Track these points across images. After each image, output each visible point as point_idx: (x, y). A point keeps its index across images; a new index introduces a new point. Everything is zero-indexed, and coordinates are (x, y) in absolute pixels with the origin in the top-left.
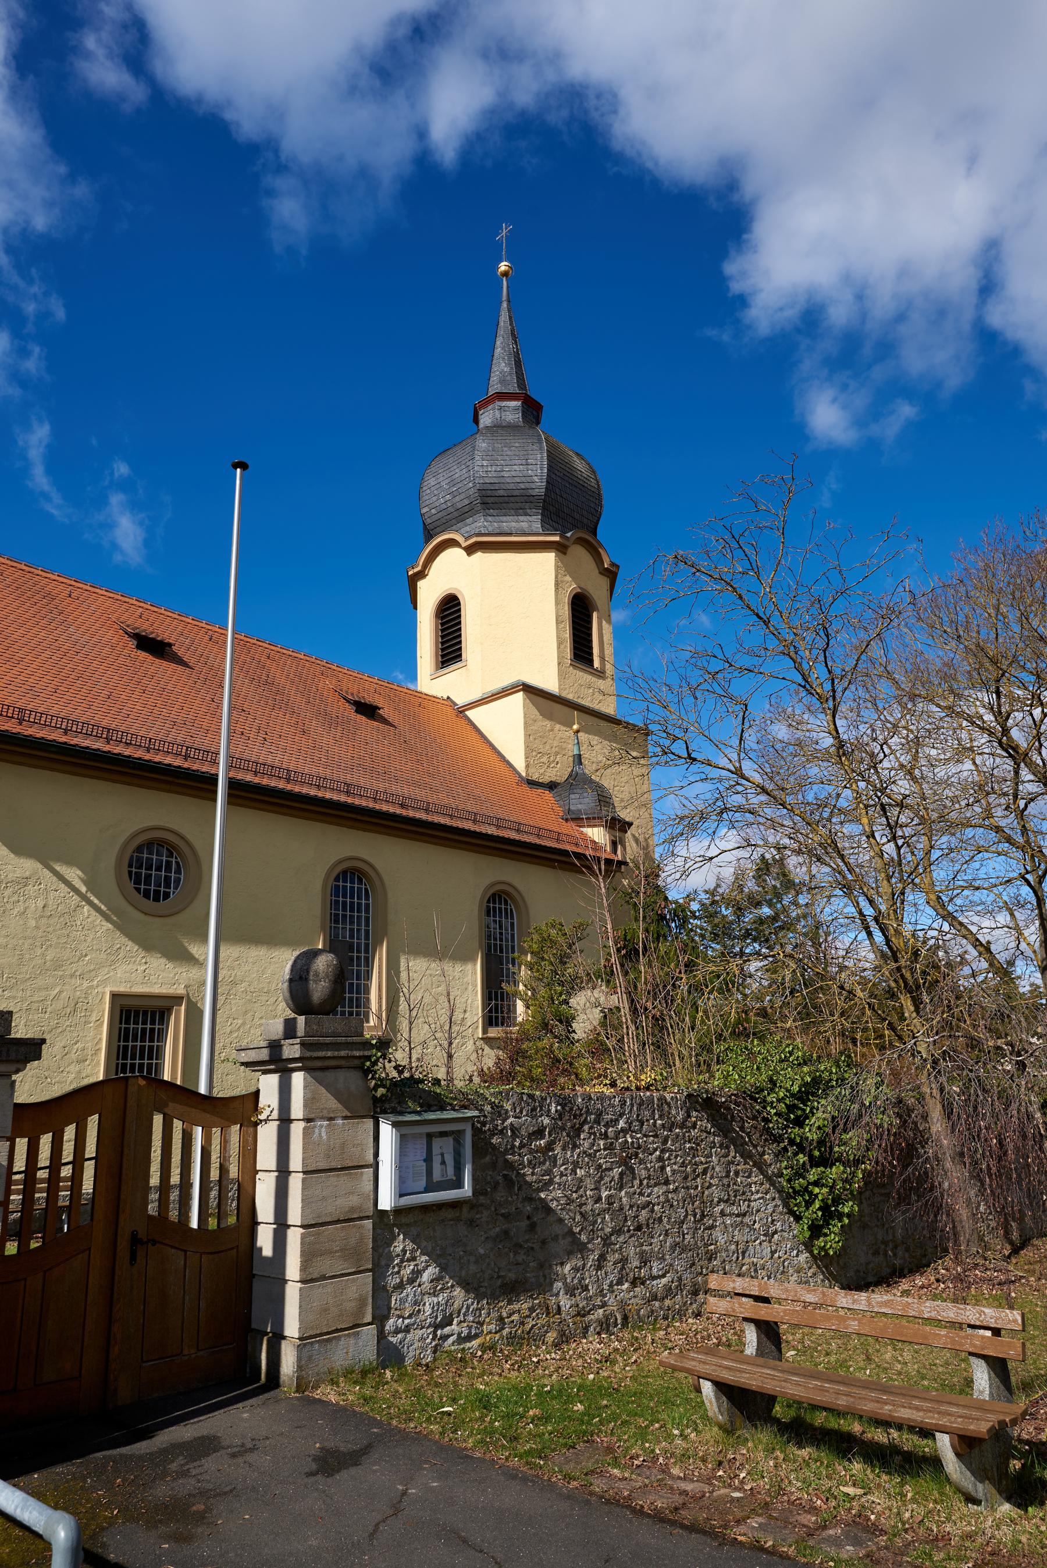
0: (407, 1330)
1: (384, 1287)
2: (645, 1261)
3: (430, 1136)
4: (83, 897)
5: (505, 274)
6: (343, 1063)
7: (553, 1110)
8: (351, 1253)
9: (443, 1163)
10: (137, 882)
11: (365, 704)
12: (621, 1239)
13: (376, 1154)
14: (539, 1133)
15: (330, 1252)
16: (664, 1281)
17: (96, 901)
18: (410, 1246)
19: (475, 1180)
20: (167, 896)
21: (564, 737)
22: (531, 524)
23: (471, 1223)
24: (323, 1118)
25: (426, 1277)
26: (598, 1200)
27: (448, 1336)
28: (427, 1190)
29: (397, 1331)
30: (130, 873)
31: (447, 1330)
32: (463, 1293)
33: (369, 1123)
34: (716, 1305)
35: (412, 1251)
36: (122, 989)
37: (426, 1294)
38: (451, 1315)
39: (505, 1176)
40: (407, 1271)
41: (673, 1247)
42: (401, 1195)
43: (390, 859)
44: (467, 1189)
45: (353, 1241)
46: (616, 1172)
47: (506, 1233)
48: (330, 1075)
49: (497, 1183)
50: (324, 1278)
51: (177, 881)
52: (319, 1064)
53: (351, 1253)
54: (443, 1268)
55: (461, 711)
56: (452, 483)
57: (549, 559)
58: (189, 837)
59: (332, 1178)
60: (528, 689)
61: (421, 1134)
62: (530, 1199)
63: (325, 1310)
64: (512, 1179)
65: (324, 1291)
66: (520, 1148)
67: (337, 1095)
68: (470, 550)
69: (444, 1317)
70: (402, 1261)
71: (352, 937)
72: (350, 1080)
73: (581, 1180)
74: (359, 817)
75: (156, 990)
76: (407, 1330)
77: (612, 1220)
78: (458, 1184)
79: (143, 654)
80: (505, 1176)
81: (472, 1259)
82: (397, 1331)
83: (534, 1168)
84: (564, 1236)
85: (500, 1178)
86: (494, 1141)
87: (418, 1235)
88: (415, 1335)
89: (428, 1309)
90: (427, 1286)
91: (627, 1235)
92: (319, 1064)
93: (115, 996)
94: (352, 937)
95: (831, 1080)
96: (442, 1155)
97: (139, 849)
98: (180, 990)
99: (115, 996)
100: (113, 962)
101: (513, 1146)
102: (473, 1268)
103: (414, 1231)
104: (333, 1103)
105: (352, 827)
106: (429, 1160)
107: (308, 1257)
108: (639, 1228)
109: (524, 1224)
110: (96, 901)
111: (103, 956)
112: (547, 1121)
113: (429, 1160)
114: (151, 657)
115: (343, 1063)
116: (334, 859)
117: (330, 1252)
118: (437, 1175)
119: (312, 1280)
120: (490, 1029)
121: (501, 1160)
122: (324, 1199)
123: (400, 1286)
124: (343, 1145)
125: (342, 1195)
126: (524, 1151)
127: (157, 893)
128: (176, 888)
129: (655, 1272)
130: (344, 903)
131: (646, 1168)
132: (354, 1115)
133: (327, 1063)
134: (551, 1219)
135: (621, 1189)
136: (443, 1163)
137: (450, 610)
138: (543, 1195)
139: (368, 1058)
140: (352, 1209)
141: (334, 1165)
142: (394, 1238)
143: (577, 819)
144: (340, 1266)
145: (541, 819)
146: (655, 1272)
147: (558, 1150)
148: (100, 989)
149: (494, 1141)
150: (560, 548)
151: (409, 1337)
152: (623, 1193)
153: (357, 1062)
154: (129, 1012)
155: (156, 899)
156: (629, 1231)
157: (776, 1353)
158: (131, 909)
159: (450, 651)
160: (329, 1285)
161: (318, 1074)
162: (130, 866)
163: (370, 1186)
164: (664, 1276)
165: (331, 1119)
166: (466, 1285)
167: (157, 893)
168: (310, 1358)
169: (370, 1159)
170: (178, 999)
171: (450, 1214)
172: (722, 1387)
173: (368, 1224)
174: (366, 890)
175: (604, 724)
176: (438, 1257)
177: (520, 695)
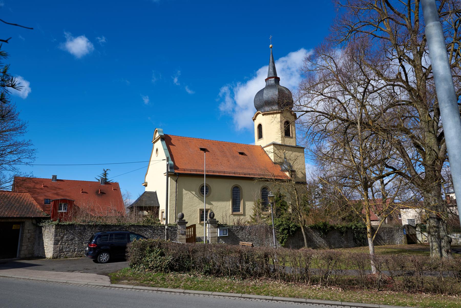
5: (271, 48)
8: (216, 240)
21: (281, 153)
22: (275, 107)
43: (243, 185)
53: (216, 240)
55: (263, 148)
56: (260, 100)
57: (279, 115)
60: (274, 144)
64: (234, 234)
68: (263, 115)
72: (214, 225)
98: (209, 208)
107: (211, 240)
125: (214, 235)
137: (260, 126)
143: (283, 171)
145: (277, 171)
150: (281, 113)
159: (260, 136)
175: (292, 148)
177: (272, 147)
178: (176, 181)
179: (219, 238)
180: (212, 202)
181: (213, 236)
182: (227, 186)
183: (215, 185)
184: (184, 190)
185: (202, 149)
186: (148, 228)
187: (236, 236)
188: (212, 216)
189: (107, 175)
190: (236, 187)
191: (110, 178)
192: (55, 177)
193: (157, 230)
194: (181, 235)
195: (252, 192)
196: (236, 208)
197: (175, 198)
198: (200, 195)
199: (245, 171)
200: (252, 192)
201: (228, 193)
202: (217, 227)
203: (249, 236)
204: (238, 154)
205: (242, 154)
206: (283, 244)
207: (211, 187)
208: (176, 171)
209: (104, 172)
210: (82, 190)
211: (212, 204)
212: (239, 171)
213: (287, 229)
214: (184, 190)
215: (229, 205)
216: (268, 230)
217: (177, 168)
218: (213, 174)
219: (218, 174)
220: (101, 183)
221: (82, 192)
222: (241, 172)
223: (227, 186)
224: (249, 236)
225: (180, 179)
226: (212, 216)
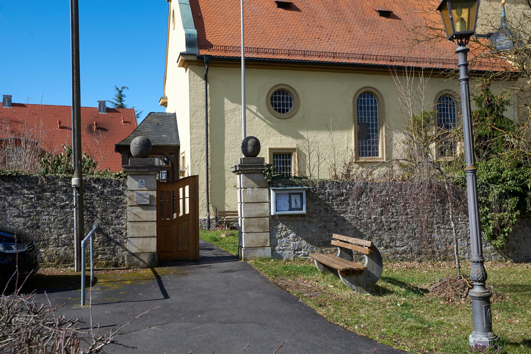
0: (284, 250)
1: (275, 237)
2: (392, 240)
3: (290, 194)
4: (255, 114)
6: (256, 171)
7: (348, 187)
8: (263, 227)
9: (296, 202)
10: (276, 106)
11: (384, 11)
12: (381, 232)
13: (270, 199)
14: (342, 195)
15: (254, 226)
16: (402, 248)
17: (260, 115)
18: (284, 227)
19: (307, 208)
20: (287, 110)
23: (309, 222)
24: (250, 188)
25: (291, 236)
26: (370, 218)
27: (300, 254)
28: (289, 210)
29: (280, 250)
30: (272, 103)
31: (300, 252)
32: (306, 242)
33: (267, 190)
34: (333, 242)
35: (285, 228)
36: (273, 146)
37: (289, 241)
38: (301, 248)
39: (325, 208)
40: (284, 233)
41: (408, 238)
42: (277, 211)
44: (304, 211)
45: (262, 223)
46: (380, 209)
47: (325, 226)
48: (252, 175)
49: (321, 210)
50: (252, 232)
51: (291, 104)
52: (247, 172)
53: (263, 227)
54: (298, 234)
58: (293, 86)
59: (254, 205)
61: (286, 193)
62: (336, 216)
63: (253, 241)
64: (328, 209)
65: (250, 236)
66: (332, 199)
67: (254, 181)
69: (298, 248)
70: (281, 231)
71: (369, 121)
72: (259, 177)
73: (361, 211)
74: (367, 69)
75: (286, 146)
76: (284, 250)
77: (376, 226)
78: (302, 209)
79: (280, 10)
80: (325, 208)
81: (310, 233)
82: (280, 250)
83: (338, 206)
84: (352, 229)
85: (322, 209)
86: (320, 197)
87: (287, 224)
88: (286, 252)
89: (292, 245)
90: (291, 239)
91: (384, 231)
92: (247, 172)
93: (270, 149)
94: (369, 121)
95: (507, 177)
96: (296, 200)
97: (275, 93)
98: (294, 146)
99: (270, 149)
100: (269, 137)
101: (329, 199)
102: (310, 235)
103: (286, 222)
104: (253, 183)
105: (366, 74)
106: (290, 202)
108: (390, 229)
109: (333, 224)
110: (260, 115)
111: (265, 135)
112: (345, 191)
113: (290, 202)
114: (284, 10)
115: (256, 171)
116: (358, 89)
117: (254, 226)
118: (293, 206)
119: (248, 233)
120: (361, 158)
121: (323, 203)
122: (251, 211)
123: (281, 238)
124: (257, 196)
125: (257, 210)
126: (334, 200)
127: (283, 110)
128: (291, 107)
129: (398, 244)
130: (368, 107)
131: (396, 209)
132: (261, 187)
133: (249, 172)
134: (345, 223)
135: (382, 215)
136: (296, 202)
138: (342, 215)
139: (264, 170)
140: (261, 214)
141: (254, 201)
142: (279, 224)
144: (258, 230)
146: (398, 244)
147: (350, 201)
148: (265, 147)
149: (320, 197)
151: (284, 252)
152: (383, 217)
153: (260, 171)
154: (277, 155)
155: (283, 112)
156: (385, 230)
157: (350, 258)
158: (273, 117)
160: (254, 235)
161: (247, 175)
162: (272, 100)
163: (268, 208)
164: (403, 246)
165: (253, 188)
166: (307, 240)
167: (283, 110)
168: (248, 253)
169: (267, 200)
170: (294, 150)
171: (301, 218)
172: (319, 263)
173: (268, 219)
174: (375, 100)
176: (293, 230)
178: (206, 79)
179: (274, 220)
180: (302, 133)
181: (253, 214)
182: (342, 92)
183: (304, 86)
184: (226, 100)
185: (280, 5)
186: (20, 183)
187: (336, 214)
188: (250, 148)
189: (124, 99)
190: (364, 93)
191: (128, 103)
192: (7, 99)
193: (54, 191)
194: (138, 210)
195: (406, 101)
196: (366, 143)
197: (204, 121)
198: (269, 115)
199: (392, 53)
200: (406, 101)
201: (347, 107)
202: (270, 185)
203: (382, 214)
204: (377, 16)
205: (386, 14)
206: (498, 243)
207: (299, 93)
208: (203, 52)
209: (117, 92)
210: (60, 122)
211: (302, 137)
212: (374, 51)
213: (514, 194)
214: (226, 100)
215: (349, 140)
216: (446, 197)
217: (208, 46)
218: (303, 58)
219: (316, 59)
220: (100, 111)
221: (60, 128)
222: (377, 53)
223: (342, 92)
224: (382, 214)
225: (215, 73)
226: (250, 148)
